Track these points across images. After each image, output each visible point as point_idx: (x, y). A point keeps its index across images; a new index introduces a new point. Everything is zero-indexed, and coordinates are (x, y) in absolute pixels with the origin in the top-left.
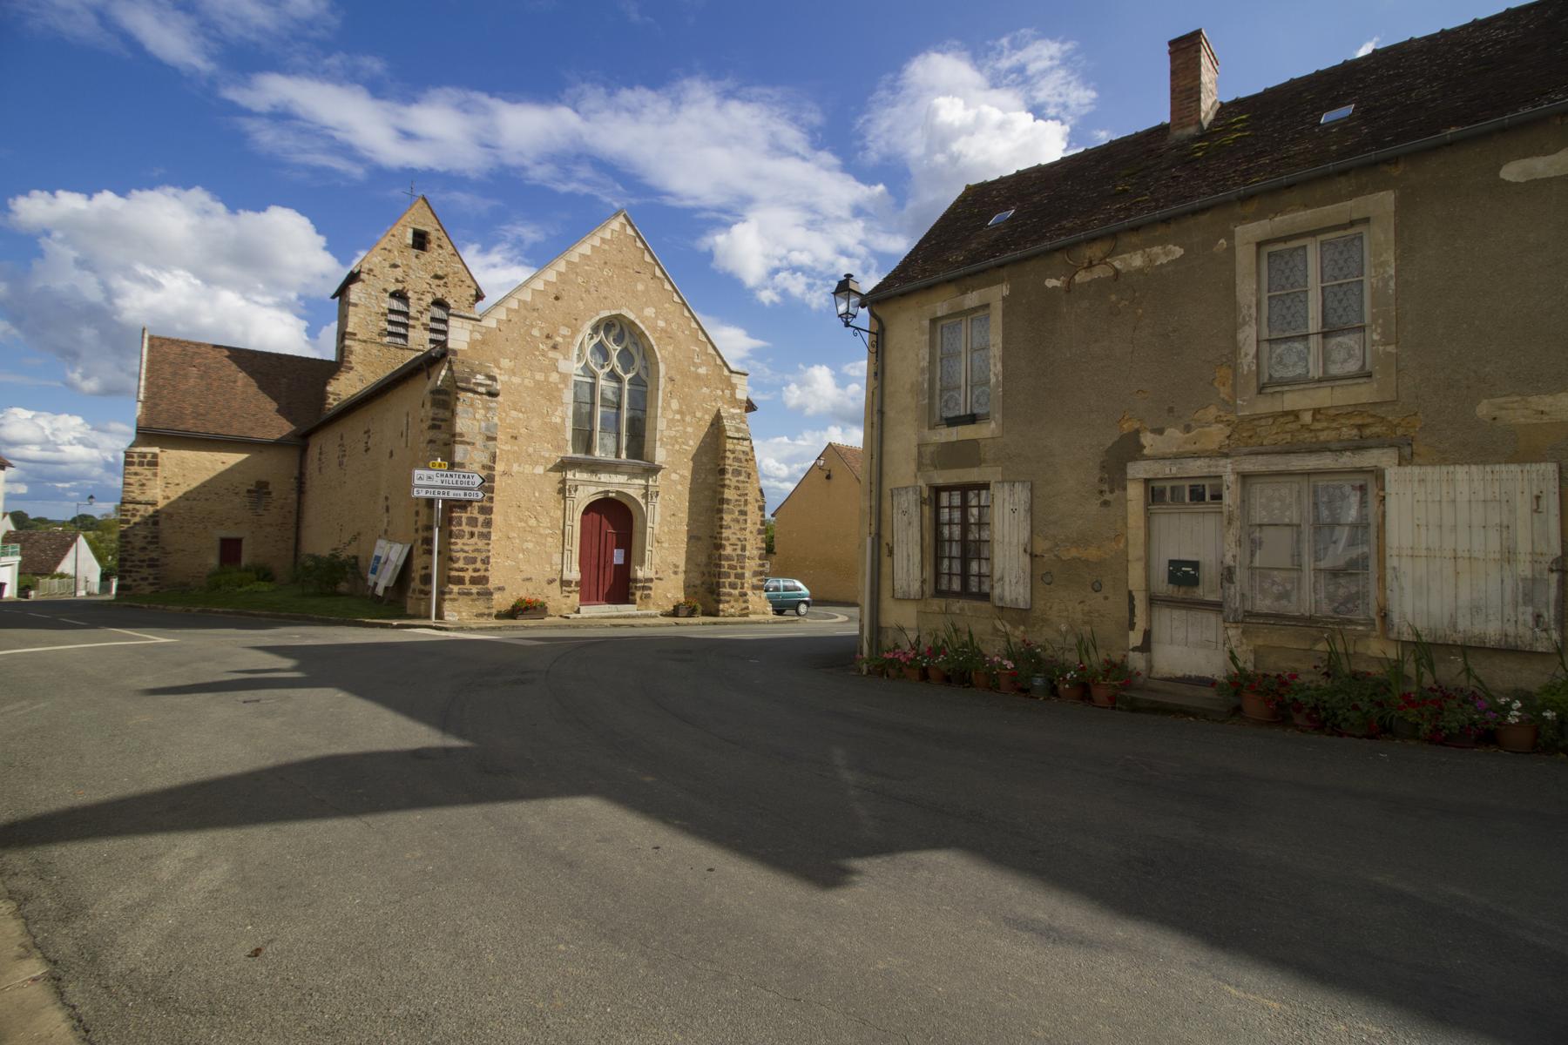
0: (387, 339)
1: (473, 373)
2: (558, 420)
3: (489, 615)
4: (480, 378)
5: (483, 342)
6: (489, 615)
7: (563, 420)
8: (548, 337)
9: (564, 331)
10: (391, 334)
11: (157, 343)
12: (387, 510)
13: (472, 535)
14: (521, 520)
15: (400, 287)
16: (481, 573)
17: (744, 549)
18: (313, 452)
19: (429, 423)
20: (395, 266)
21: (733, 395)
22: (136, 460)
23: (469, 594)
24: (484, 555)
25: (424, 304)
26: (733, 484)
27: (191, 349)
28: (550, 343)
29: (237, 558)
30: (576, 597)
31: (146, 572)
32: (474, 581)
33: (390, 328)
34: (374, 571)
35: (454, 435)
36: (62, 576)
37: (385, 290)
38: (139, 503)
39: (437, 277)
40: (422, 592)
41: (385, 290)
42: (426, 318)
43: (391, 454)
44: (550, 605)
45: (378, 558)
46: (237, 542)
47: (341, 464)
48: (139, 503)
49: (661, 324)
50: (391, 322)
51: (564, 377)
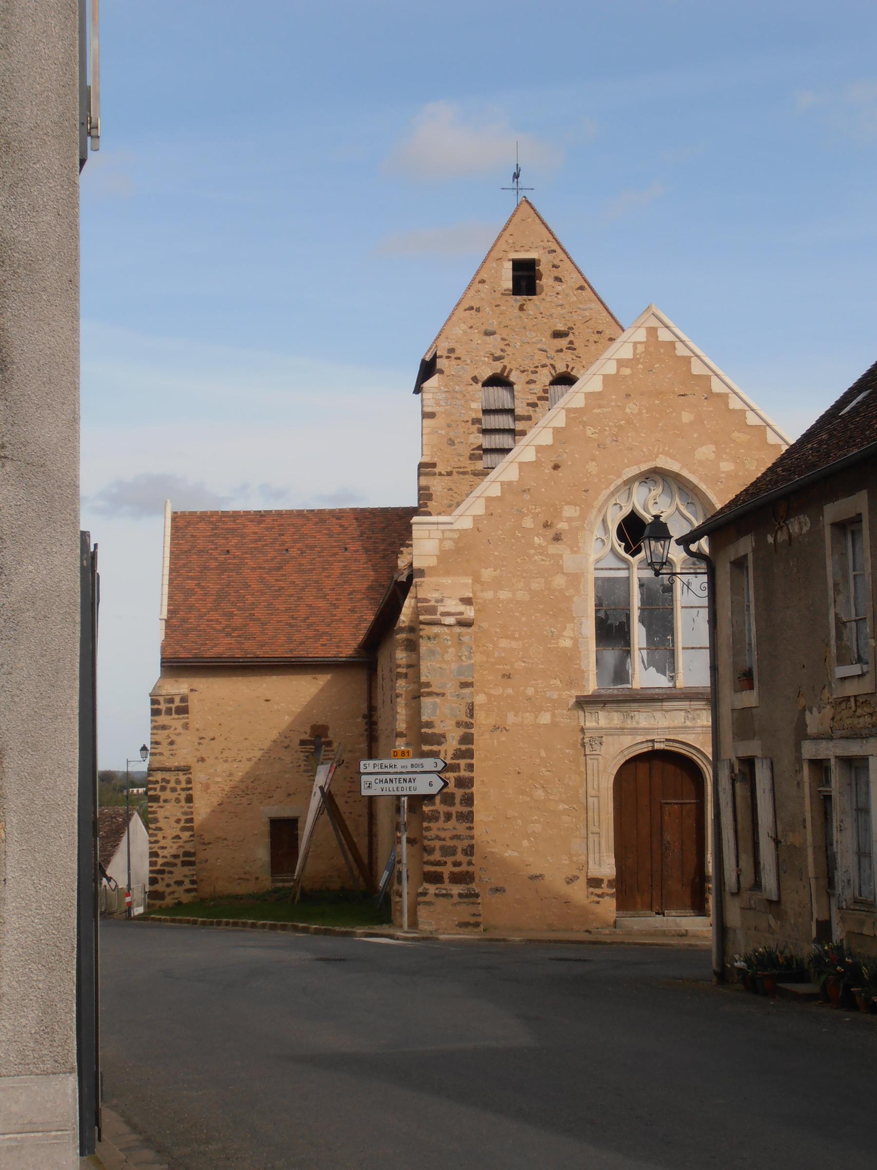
2: (567, 643)
8: (546, 525)
9: (569, 511)
13: (448, 817)
15: (497, 367)
16: (464, 868)
22: (163, 706)
23: (448, 896)
24: (466, 843)
25: (537, 388)
28: (550, 533)
32: (456, 879)
35: (421, 685)
37: (475, 379)
38: (168, 770)
39: (558, 335)
41: (475, 379)
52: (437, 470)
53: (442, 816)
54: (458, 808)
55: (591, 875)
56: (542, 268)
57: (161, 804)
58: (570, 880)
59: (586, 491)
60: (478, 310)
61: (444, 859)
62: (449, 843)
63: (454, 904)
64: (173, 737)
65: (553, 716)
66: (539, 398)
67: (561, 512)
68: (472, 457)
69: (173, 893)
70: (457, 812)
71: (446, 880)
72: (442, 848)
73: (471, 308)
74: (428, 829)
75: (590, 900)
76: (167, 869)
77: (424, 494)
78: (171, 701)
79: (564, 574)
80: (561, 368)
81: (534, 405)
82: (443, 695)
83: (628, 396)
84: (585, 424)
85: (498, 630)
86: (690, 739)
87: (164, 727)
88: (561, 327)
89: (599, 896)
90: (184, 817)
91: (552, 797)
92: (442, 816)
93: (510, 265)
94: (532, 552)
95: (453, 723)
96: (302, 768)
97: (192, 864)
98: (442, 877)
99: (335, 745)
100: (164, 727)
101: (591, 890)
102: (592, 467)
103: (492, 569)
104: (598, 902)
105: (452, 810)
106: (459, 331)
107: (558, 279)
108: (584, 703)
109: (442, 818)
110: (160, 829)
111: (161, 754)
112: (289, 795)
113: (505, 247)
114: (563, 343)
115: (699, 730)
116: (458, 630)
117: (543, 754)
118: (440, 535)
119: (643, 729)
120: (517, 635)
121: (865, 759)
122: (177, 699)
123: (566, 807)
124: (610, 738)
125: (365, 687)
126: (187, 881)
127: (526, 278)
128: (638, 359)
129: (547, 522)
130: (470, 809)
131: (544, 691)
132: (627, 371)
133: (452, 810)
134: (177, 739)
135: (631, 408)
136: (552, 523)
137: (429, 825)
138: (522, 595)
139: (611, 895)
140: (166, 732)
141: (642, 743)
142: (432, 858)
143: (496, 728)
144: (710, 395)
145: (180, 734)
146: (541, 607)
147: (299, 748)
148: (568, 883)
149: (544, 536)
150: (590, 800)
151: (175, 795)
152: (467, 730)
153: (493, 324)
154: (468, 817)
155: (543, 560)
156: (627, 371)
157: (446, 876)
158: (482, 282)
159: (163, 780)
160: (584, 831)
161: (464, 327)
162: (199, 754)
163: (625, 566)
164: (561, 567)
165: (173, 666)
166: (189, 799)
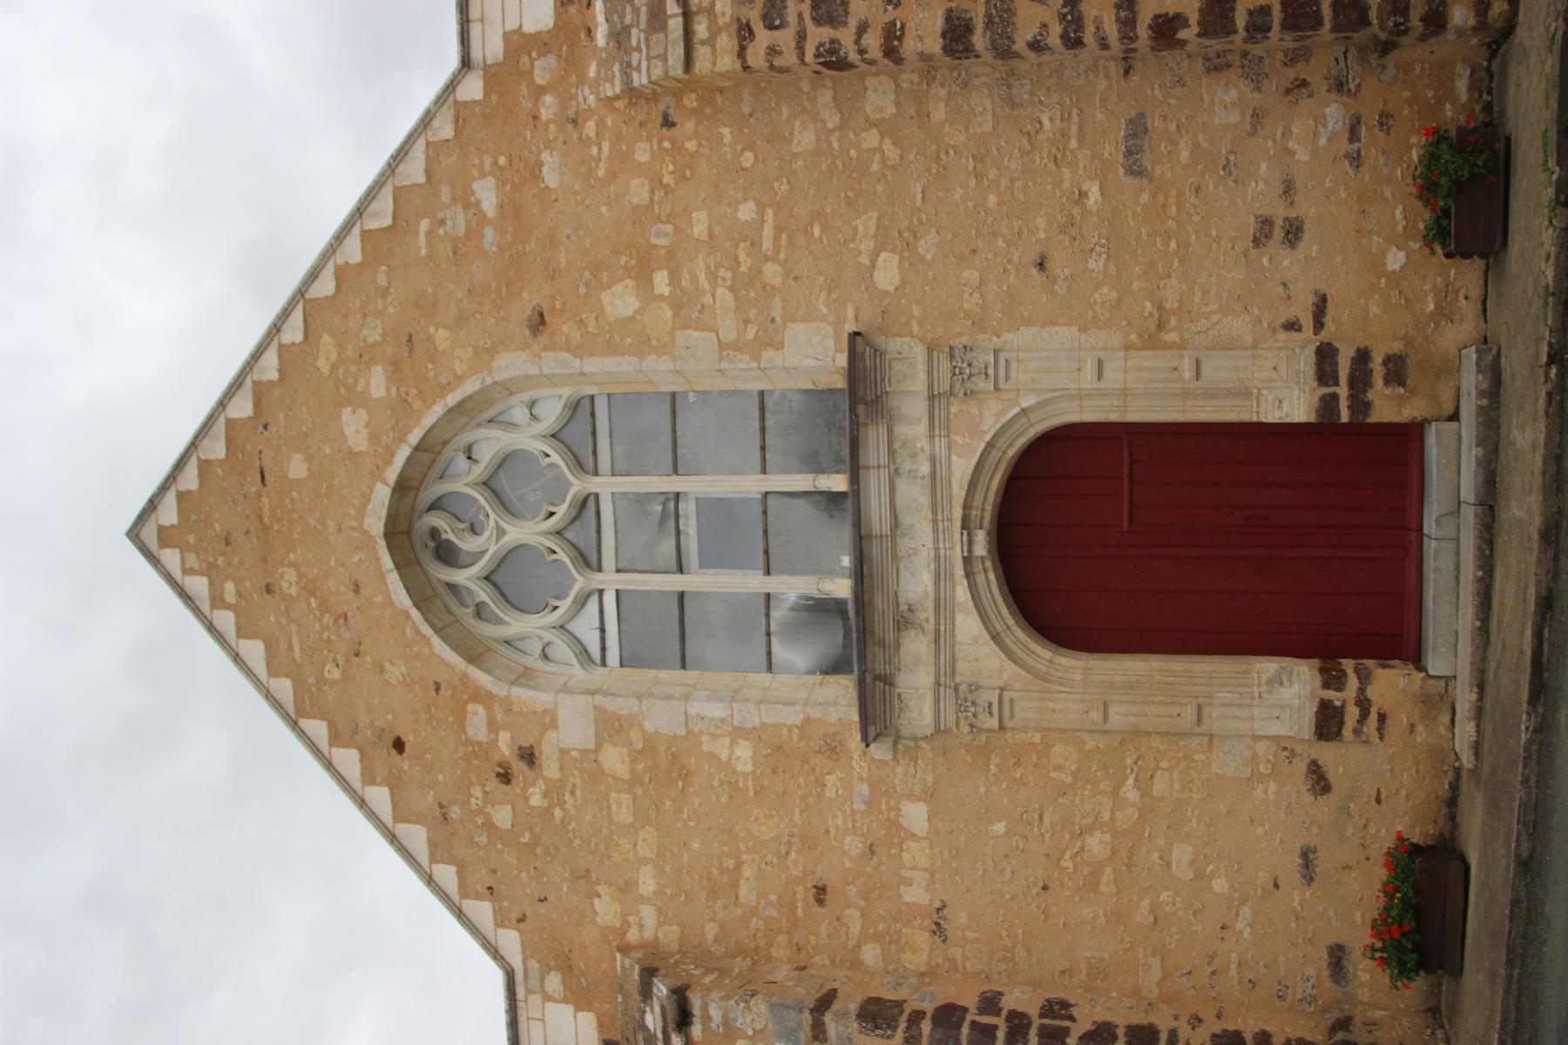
5: (565, 966)
8: (505, 777)
14: (1093, 883)
30: (1390, 684)
49: (377, 383)
51: (610, 727)
58: (1320, 782)
65: (910, 797)
67: (479, 743)
79: (597, 750)
83: (269, 589)
84: (322, 681)
85: (720, 903)
86: (962, 468)
89: (1364, 715)
91: (1106, 816)
94: (558, 812)
101: (1347, 732)
102: (396, 672)
103: (596, 900)
104: (1382, 718)
108: (876, 714)
117: (1000, 828)
118: (536, 999)
119: (937, 583)
120: (731, 863)
123: (1130, 781)
124: (962, 667)
129: (498, 775)
131: (853, 812)
135: (288, 580)
136: (500, 765)
138: (648, 836)
139: (1364, 678)
143: (938, 929)
144: (260, 421)
146: (668, 803)
148: (1326, 789)
149: (526, 786)
155: (573, 793)
156: (230, 588)
160: (1194, 742)
164: (584, 752)
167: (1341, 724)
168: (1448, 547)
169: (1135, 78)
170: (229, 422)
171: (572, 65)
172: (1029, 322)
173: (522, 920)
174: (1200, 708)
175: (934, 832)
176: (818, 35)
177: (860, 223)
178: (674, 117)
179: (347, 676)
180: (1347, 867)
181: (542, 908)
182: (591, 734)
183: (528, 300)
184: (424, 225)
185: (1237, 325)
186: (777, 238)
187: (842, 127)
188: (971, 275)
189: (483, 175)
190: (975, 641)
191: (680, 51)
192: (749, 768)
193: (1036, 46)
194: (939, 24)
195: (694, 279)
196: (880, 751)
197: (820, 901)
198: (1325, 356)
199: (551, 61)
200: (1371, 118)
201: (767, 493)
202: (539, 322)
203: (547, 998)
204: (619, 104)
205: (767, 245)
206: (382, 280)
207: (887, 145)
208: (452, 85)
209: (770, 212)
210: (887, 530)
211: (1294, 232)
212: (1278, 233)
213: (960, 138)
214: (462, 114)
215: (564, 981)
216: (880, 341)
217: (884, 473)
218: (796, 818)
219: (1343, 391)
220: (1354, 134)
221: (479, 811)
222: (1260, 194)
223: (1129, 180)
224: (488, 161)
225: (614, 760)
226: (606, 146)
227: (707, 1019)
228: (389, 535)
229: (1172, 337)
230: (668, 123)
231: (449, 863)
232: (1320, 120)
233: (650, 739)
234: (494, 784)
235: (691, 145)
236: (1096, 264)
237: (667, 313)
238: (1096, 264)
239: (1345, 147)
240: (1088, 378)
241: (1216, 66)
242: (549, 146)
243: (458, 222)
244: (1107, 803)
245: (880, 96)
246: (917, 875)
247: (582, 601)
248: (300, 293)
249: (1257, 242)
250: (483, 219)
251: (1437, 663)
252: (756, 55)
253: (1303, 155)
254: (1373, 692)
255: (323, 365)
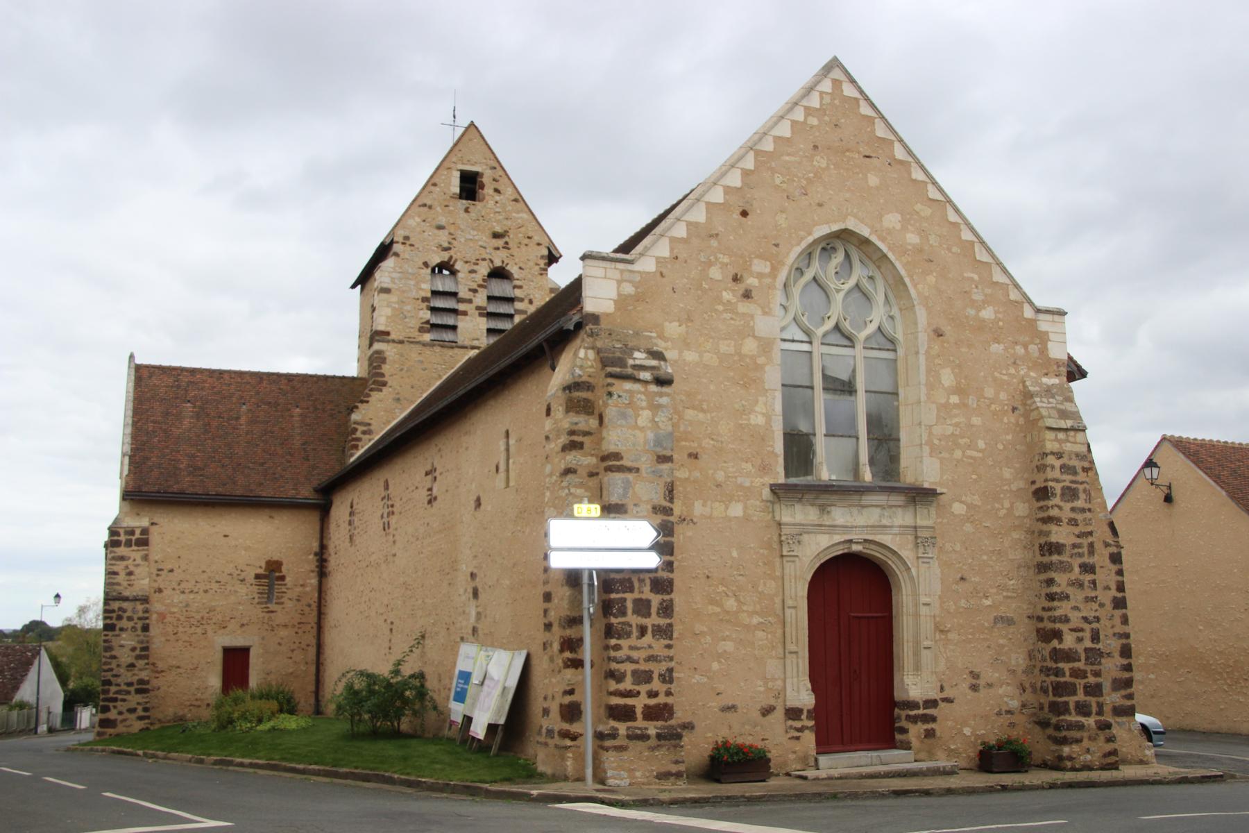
0: (427, 337)
1: (629, 351)
3: (678, 775)
4: (640, 357)
5: (638, 298)
6: (678, 775)
7: (768, 418)
9: (761, 266)
10: (435, 327)
11: (146, 373)
12: (475, 594)
13: (643, 631)
14: (713, 602)
15: (445, 256)
16: (661, 699)
17: (1095, 637)
18: (339, 511)
19: (564, 439)
20: (440, 228)
21: (1043, 351)
22: (123, 538)
23: (644, 737)
24: (663, 667)
26: (1066, 514)
27: (185, 379)
28: (740, 288)
29: (243, 681)
30: (809, 738)
31: (134, 699)
32: (653, 713)
33: (437, 320)
34: (461, 697)
36: (22, 706)
38: (126, 599)
39: (496, 236)
40: (565, 735)
41: (426, 264)
42: (481, 299)
43: (478, 503)
44: (773, 754)
45: (466, 676)
46: (244, 652)
47: (386, 527)
48: (126, 599)
49: (912, 238)
50: (434, 310)
51: (766, 345)
52: (390, 338)
53: (634, 630)
54: (654, 620)
55: (790, 704)
56: (486, 180)
57: (117, 632)
58: (767, 711)
59: (777, 245)
60: (430, 207)
61: (637, 688)
62: (643, 666)
63: (652, 749)
64: (132, 568)
65: (745, 508)
66: (480, 286)
68: (421, 330)
69: (125, 720)
70: (653, 625)
71: (639, 715)
72: (634, 673)
73: (425, 205)
74: (617, 648)
75: (789, 735)
76: (120, 697)
77: (375, 362)
78: (132, 533)
79: (754, 336)
80: (498, 263)
81: (475, 291)
82: (638, 470)
86: (886, 539)
87: (122, 558)
88: (498, 229)
89: (799, 730)
90: (139, 646)
91: (745, 608)
92: (634, 630)
93: (458, 174)
94: (720, 308)
95: (649, 507)
96: (257, 600)
97: (145, 691)
98: (634, 712)
99: (288, 579)
100: (122, 558)
101: (790, 723)
102: (781, 220)
104: (798, 738)
105: (648, 622)
106: (413, 222)
107: (497, 191)
109: (635, 633)
110: (114, 657)
111: (118, 584)
112: (243, 625)
113: (454, 159)
114: (500, 243)
115: (896, 530)
116: (653, 388)
117: (735, 554)
118: (617, 275)
120: (705, 407)
121: (1039, 572)
122: (138, 532)
125: (318, 528)
126: (140, 708)
127: (470, 186)
128: (825, 110)
130: (668, 621)
132: (813, 121)
133: (648, 622)
134: (137, 571)
135: (821, 161)
137: (619, 642)
138: (711, 359)
140: (125, 563)
141: (839, 543)
142: (621, 687)
145: (137, 565)
147: (254, 581)
148: (764, 715)
149: (733, 291)
150: (788, 612)
151: (131, 624)
152: (666, 518)
153: (442, 221)
154: (664, 632)
156: (813, 121)
157: (639, 711)
158: (435, 185)
159: (120, 609)
160: (780, 650)
161: (417, 219)
162: (156, 585)
163: (805, 338)
164: (753, 329)
165: (135, 496)
166: (146, 628)
167: (794, 719)
168: (869, 761)
169: (1027, 621)
170: (892, 142)
171: (1035, 365)
172: (942, 572)
173: (662, 274)
174: (796, 653)
175: (730, 519)
176: (1058, 488)
177: (976, 497)
178: (1017, 412)
179: (777, 187)
180: (730, 728)
181: (669, 289)
182: (762, 334)
183: (947, 329)
184: (976, 277)
185: (942, 666)
186: (971, 457)
187: (1011, 491)
188: (958, 547)
189: (996, 312)
190: (818, 544)
191: (1055, 426)
192: (753, 422)
193: (1050, 582)
194: (1062, 541)
195: (956, 416)
196: (766, 493)
197: (690, 455)
198: (932, 703)
199: (1036, 354)
200: (1014, 719)
201: (858, 439)
202: (939, 334)
203: (619, 282)
204: (1021, 386)
205: (969, 453)
206: (955, 249)
207: (1004, 511)
208: (1030, 303)
209: (980, 455)
210: (863, 503)
211: (974, 688)
212: (974, 682)
213: (1007, 544)
214: (1017, 305)
215: (630, 295)
216: (935, 504)
217: (884, 503)
218: (731, 446)
219: (921, 711)
220: (1009, 712)
221: (717, 259)
222: (989, 675)
223: (992, 618)
224: (1000, 316)
225: (750, 346)
226: (1005, 378)
227: (661, 395)
228: (846, 231)
229: (938, 637)
230: (1014, 409)
231: (688, 233)
232: (1012, 698)
233: (759, 368)
234: (731, 271)
235: (1005, 420)
236: (963, 603)
237: (943, 401)
238: (963, 603)
239: (1004, 708)
240: (924, 599)
241: (1031, 655)
242: (1006, 349)
243: (978, 297)
244: (751, 609)
245: (1022, 509)
246: (708, 509)
247: (807, 332)
248: (950, 201)
249: (971, 672)
250: (978, 310)
251: (824, 760)
252: (1051, 460)
253: (1001, 691)
254: (807, 732)
255: (918, 207)
